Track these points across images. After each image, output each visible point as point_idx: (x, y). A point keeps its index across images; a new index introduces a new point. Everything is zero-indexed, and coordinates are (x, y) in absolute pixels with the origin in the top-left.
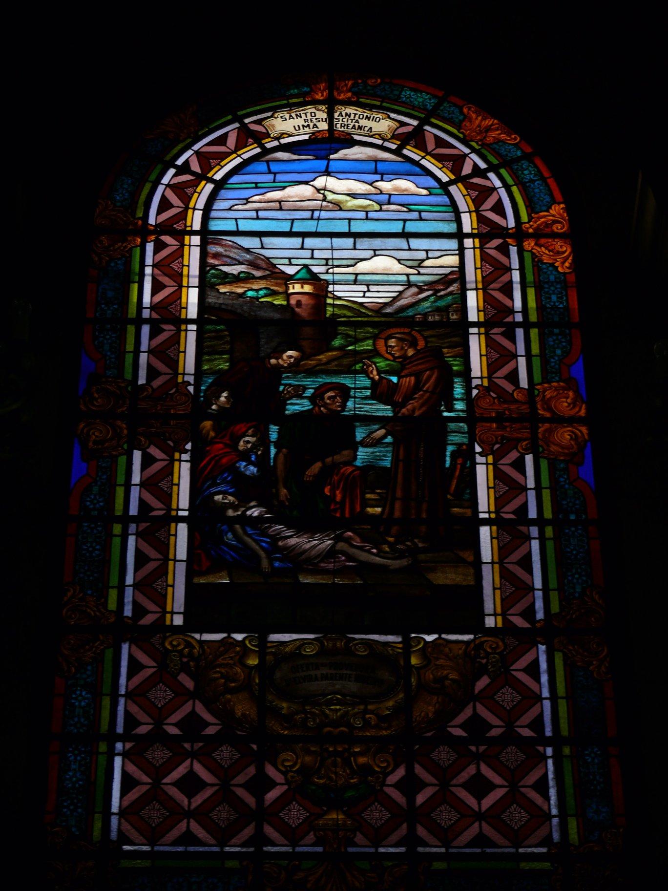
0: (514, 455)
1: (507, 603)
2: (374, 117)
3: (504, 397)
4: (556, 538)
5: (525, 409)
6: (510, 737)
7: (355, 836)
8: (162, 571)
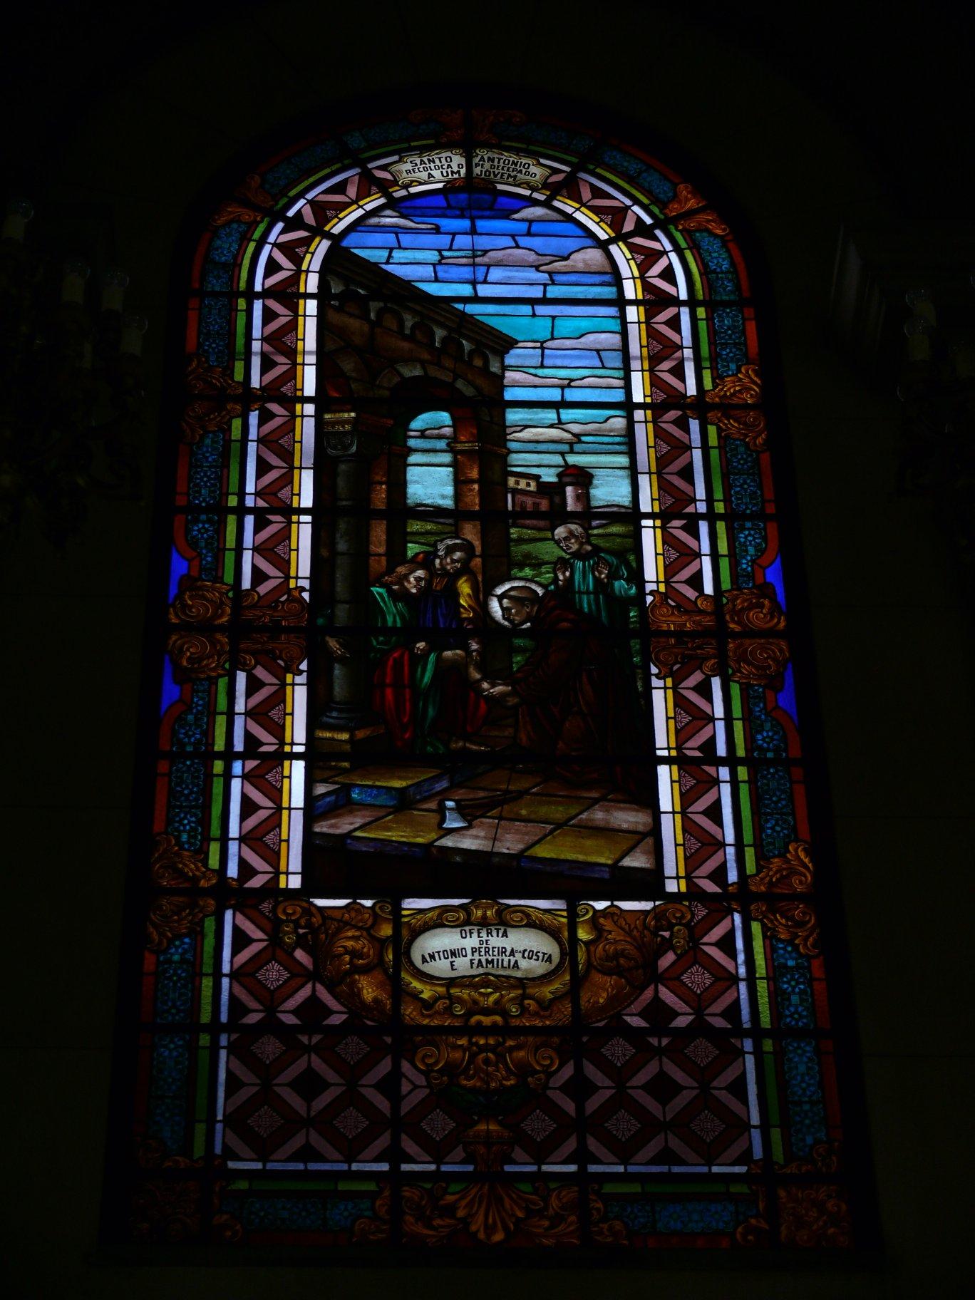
0: (696, 678)
1: (692, 862)
2: (521, 162)
3: (685, 606)
4: (751, 781)
5: (708, 621)
6: (700, 1027)
7: (513, 1151)
8: (274, 822)
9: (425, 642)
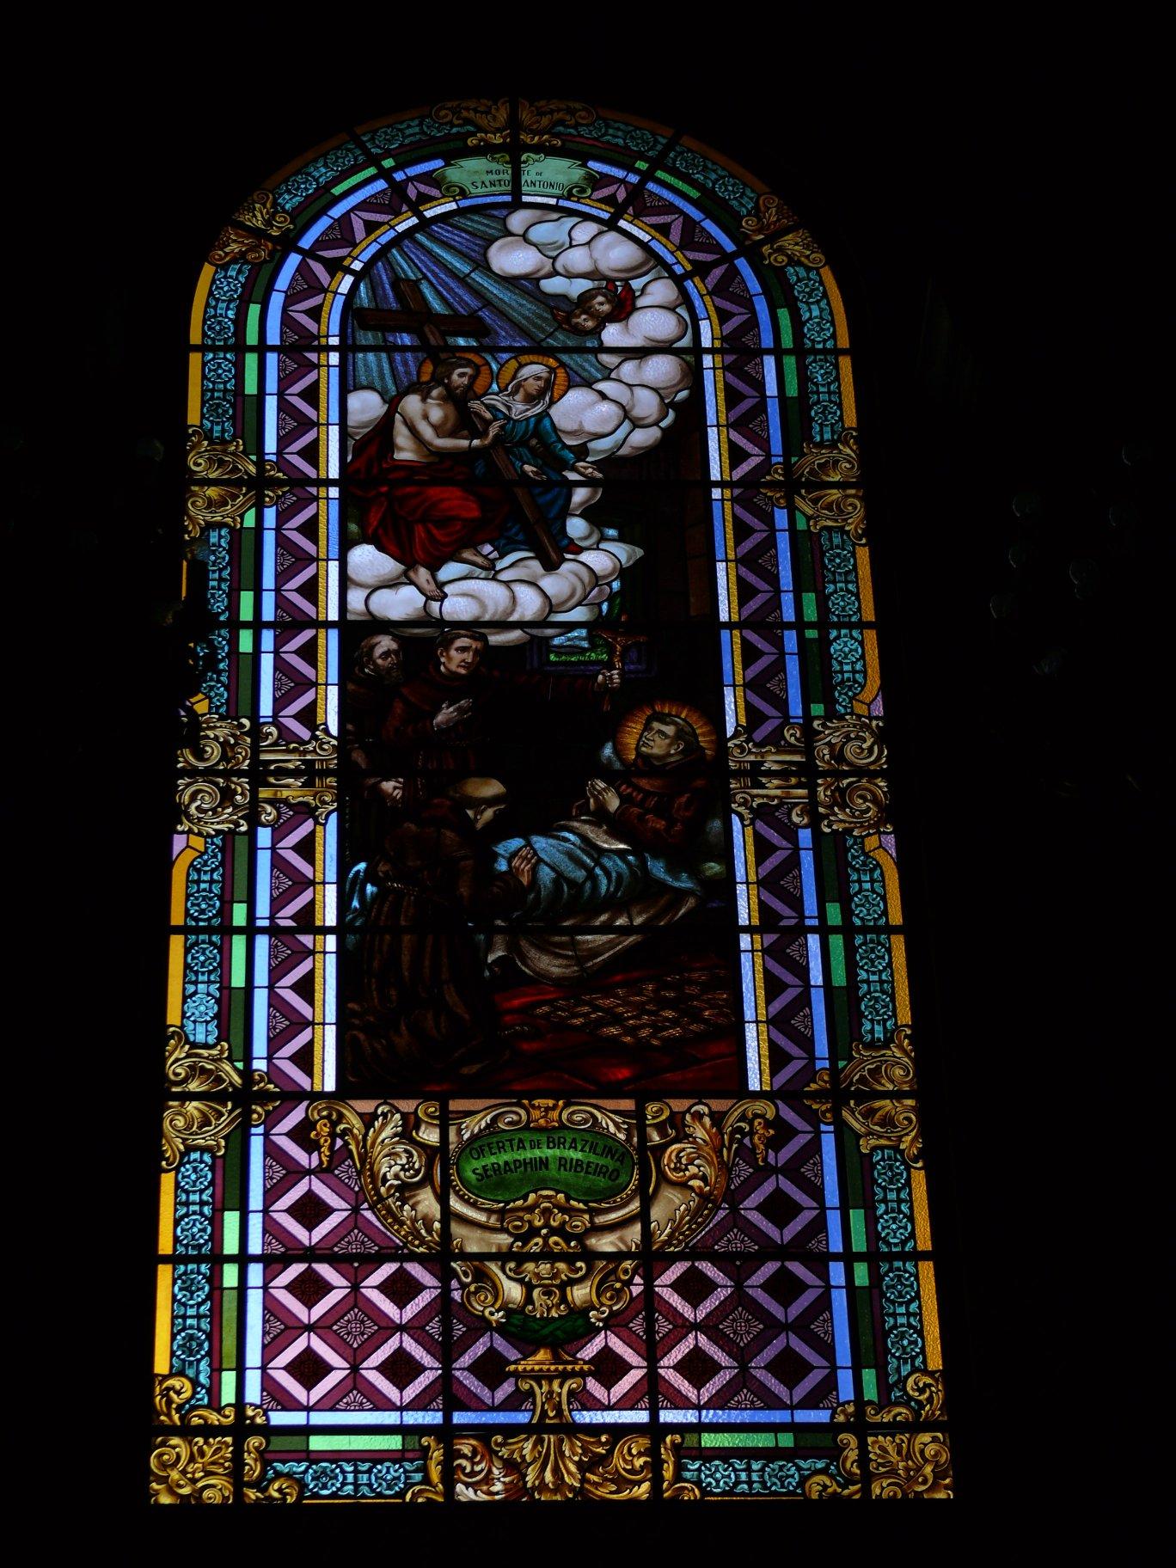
9: (243, 1082)
